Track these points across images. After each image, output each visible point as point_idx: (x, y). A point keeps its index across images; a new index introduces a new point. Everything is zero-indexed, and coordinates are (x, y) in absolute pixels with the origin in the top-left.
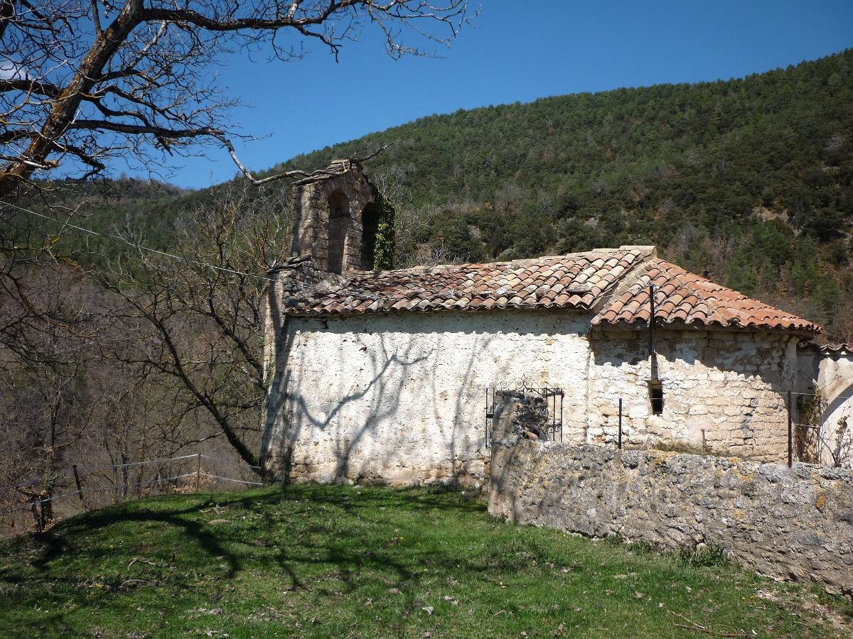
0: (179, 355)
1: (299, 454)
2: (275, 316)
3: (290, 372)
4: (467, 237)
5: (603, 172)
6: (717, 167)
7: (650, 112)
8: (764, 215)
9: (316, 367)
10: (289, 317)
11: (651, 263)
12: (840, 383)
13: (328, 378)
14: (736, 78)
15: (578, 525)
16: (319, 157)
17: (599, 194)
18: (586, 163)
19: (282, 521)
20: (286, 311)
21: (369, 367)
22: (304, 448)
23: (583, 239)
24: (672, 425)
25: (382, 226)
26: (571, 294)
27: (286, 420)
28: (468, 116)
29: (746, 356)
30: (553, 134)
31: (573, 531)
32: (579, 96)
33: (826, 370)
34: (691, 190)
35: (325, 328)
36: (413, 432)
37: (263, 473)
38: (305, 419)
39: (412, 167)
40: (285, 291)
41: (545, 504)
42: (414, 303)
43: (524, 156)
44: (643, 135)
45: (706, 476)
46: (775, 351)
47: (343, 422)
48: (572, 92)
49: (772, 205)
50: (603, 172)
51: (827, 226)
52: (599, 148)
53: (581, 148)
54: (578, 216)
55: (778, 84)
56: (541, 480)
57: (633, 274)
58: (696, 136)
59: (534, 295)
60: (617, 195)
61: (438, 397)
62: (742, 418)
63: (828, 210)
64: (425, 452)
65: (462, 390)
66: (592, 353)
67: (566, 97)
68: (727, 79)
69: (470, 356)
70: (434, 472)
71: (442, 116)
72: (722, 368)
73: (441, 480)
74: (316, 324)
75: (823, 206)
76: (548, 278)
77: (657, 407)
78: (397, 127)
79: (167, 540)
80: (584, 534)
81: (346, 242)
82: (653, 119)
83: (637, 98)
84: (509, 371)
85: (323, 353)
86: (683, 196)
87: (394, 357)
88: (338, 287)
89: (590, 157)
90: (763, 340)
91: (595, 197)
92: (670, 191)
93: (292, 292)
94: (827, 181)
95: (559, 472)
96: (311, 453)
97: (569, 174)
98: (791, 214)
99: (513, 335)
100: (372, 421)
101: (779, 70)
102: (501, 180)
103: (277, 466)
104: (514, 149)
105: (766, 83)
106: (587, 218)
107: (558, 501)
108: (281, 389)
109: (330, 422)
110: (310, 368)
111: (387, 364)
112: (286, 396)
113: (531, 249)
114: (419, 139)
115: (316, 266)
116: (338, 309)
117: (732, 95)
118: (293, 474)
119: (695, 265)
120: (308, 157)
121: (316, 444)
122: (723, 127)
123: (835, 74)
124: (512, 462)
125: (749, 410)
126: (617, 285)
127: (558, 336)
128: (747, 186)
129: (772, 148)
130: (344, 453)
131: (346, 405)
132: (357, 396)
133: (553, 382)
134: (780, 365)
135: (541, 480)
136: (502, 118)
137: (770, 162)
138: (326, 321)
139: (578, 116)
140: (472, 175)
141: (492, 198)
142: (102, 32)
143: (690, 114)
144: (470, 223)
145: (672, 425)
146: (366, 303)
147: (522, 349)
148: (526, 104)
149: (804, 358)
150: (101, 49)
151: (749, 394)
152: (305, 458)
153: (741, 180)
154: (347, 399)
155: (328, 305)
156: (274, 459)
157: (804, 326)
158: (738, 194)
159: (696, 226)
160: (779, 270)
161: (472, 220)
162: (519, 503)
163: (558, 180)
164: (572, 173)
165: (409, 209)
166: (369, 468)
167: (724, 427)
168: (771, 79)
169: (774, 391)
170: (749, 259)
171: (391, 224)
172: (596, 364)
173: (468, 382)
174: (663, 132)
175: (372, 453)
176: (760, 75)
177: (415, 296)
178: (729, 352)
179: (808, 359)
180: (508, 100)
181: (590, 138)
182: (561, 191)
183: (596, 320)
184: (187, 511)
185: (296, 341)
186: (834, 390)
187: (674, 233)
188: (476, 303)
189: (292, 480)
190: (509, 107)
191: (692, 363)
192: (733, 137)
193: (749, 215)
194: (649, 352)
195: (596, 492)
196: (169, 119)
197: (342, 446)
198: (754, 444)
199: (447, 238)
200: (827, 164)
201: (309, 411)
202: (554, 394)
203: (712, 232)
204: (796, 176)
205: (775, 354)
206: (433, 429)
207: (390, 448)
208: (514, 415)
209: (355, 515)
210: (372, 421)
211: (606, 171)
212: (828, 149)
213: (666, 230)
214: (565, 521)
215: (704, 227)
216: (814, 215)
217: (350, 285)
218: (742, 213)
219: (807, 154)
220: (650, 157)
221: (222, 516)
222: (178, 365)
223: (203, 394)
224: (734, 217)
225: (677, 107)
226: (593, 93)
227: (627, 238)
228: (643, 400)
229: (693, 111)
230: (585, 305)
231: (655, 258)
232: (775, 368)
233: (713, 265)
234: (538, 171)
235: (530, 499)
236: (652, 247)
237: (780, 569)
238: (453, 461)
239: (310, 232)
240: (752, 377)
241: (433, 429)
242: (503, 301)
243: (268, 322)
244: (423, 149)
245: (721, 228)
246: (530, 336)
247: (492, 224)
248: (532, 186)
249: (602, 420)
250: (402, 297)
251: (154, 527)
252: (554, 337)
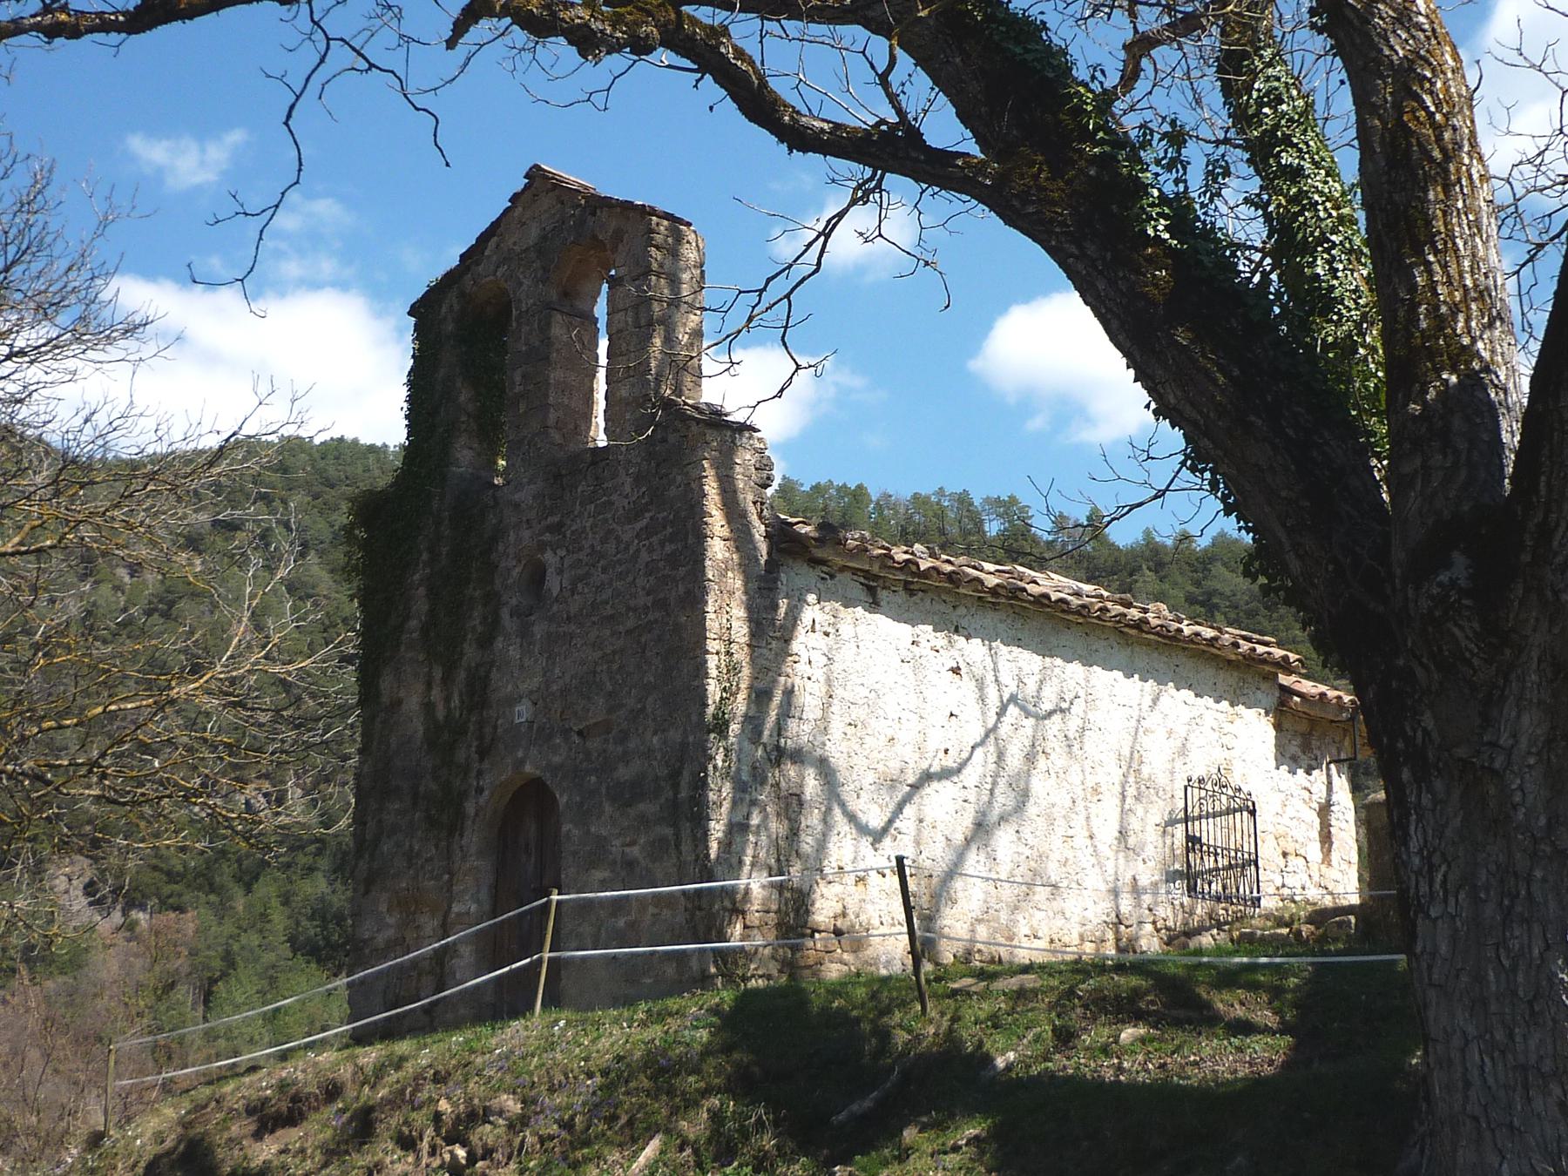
1: (824, 910)
2: (740, 536)
100: (981, 829)
127: (1241, 708)
154: (927, 777)
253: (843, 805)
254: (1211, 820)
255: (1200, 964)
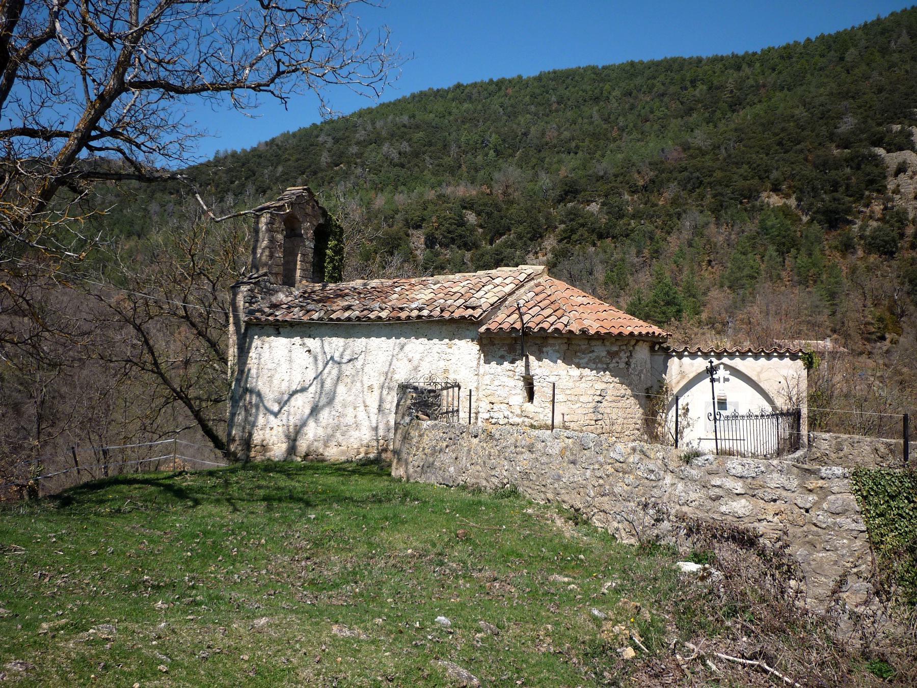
0: (156, 354)
1: (257, 437)
2: (237, 324)
3: (249, 370)
4: (462, 223)
5: (609, 152)
6: (726, 148)
7: (658, 87)
8: (772, 201)
9: (270, 366)
10: (248, 324)
11: (541, 280)
12: (683, 377)
13: (281, 374)
14: (750, 52)
15: (444, 479)
16: (305, 135)
17: (602, 177)
18: (590, 142)
19: (237, 483)
20: (246, 319)
21: (311, 367)
22: (261, 432)
23: (583, 225)
24: (540, 410)
25: (331, 243)
26: (467, 308)
27: (246, 410)
28: (466, 91)
29: (597, 357)
30: (557, 111)
31: (441, 484)
32: (585, 69)
33: (673, 367)
34: (698, 174)
35: (278, 334)
36: (348, 418)
37: (228, 455)
38: (262, 408)
39: (405, 146)
40: (245, 302)
41: (425, 467)
42: (347, 314)
43: (525, 134)
44: (652, 112)
45: (512, 440)
46: (623, 352)
47: (292, 410)
48: (577, 66)
49: (780, 190)
50: (609, 152)
51: (836, 212)
52: (605, 126)
53: (586, 126)
54: (578, 201)
55: (794, 59)
56: (424, 449)
57: (522, 290)
58: (707, 115)
59: (438, 309)
60: (620, 179)
61: (366, 390)
62: (594, 404)
63: (836, 195)
64: (355, 434)
65: (384, 383)
66: (482, 355)
67: (572, 70)
68: (741, 53)
69: (391, 357)
70: (362, 450)
71: (438, 91)
72: (578, 366)
73: (368, 456)
74: (271, 330)
75: (833, 191)
76: (455, 293)
77: (531, 396)
78: (390, 102)
79: (151, 494)
80: (447, 485)
81: (299, 258)
82: (663, 95)
83: (647, 72)
84: (419, 369)
85: (276, 354)
86: (689, 179)
87: (332, 358)
88: (290, 299)
89: (595, 136)
90: (612, 344)
91: (598, 181)
92: (675, 174)
93: (251, 303)
94: (837, 165)
95: (434, 443)
96: (267, 436)
97: (572, 154)
98: (799, 200)
99: (424, 340)
100: (315, 411)
101: (796, 43)
102: (501, 160)
103: (240, 448)
104: (515, 126)
105: (782, 57)
106: (589, 202)
107: (433, 464)
108: (242, 384)
109: (282, 411)
110: (266, 367)
111: (327, 364)
112: (246, 390)
113: (529, 235)
114: (414, 116)
115: (272, 280)
116: (287, 319)
117: (747, 70)
118: (252, 454)
119: (698, 253)
120: (294, 135)
121: (272, 429)
122: (735, 105)
123: (852, 50)
124: (406, 438)
125: (600, 398)
126: (506, 300)
127: (456, 341)
128: (755, 169)
129: (783, 130)
130: (293, 439)
131: (295, 397)
132: (303, 390)
133: (452, 378)
134: (628, 364)
135: (424, 449)
136: (502, 93)
137: (780, 144)
138: (279, 328)
139: (584, 91)
140: (469, 155)
141: (489, 181)
142: (91, 102)
143: (701, 90)
144: (465, 208)
145: (540, 410)
146: (311, 313)
147: (430, 351)
148: (529, 78)
149: (656, 357)
150: (91, 116)
151: (600, 386)
152: (263, 441)
153: (749, 163)
154: (296, 392)
155: (280, 314)
156: (237, 442)
157: (656, 334)
158: (745, 179)
159: (701, 212)
160: (784, 259)
161: (467, 205)
162: (410, 467)
163: (560, 162)
164: (576, 153)
165: (402, 192)
166: (313, 448)
167: (580, 411)
168: (787, 53)
169: (622, 383)
170: (754, 247)
171: (340, 241)
172: (485, 363)
173: (389, 377)
174: (673, 109)
175: (315, 436)
176: (776, 48)
177: (348, 308)
178: (583, 353)
179: (660, 358)
180: (510, 74)
181: (596, 116)
182: (563, 172)
183: (482, 329)
184: (165, 478)
185: (254, 345)
186: (678, 382)
187: (679, 219)
188: (394, 314)
189: (252, 459)
190: (510, 81)
191: (555, 362)
192: (745, 115)
193: (756, 200)
194: (523, 355)
195: (454, 456)
196: (144, 152)
197: (291, 430)
198: (604, 425)
199: (441, 224)
200: (838, 147)
201: (266, 403)
202: (453, 387)
203: (717, 218)
204: (806, 159)
205: (622, 354)
206: (362, 415)
207: (329, 431)
208: (409, 402)
209: (293, 479)
210: (315, 411)
211: (611, 151)
212: (839, 131)
213: (670, 216)
214: (436, 477)
215: (709, 213)
216: (823, 200)
217: (301, 296)
218: (749, 198)
219: (817, 136)
220: (658, 137)
221: (191, 481)
222: (156, 364)
223: (179, 389)
224: (741, 203)
225: (689, 83)
226: (600, 67)
227: (629, 224)
228: (519, 391)
229: (705, 87)
230: (474, 317)
231: (546, 277)
232: (622, 365)
233: (717, 253)
234: (540, 151)
235: (416, 464)
236: (542, 267)
237: (543, 496)
238: (378, 441)
239: (267, 253)
240: (602, 373)
241: (362, 415)
242: (415, 313)
243: (231, 328)
244: (418, 127)
245: (726, 213)
246: (436, 341)
247: (488, 209)
248: (533, 168)
249: (489, 407)
250: (339, 308)
251: (140, 488)
252: (453, 342)
253: (263, 403)
254: (738, 441)
255: (7, 289)
